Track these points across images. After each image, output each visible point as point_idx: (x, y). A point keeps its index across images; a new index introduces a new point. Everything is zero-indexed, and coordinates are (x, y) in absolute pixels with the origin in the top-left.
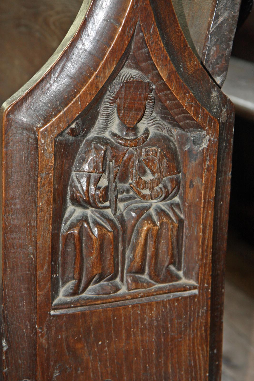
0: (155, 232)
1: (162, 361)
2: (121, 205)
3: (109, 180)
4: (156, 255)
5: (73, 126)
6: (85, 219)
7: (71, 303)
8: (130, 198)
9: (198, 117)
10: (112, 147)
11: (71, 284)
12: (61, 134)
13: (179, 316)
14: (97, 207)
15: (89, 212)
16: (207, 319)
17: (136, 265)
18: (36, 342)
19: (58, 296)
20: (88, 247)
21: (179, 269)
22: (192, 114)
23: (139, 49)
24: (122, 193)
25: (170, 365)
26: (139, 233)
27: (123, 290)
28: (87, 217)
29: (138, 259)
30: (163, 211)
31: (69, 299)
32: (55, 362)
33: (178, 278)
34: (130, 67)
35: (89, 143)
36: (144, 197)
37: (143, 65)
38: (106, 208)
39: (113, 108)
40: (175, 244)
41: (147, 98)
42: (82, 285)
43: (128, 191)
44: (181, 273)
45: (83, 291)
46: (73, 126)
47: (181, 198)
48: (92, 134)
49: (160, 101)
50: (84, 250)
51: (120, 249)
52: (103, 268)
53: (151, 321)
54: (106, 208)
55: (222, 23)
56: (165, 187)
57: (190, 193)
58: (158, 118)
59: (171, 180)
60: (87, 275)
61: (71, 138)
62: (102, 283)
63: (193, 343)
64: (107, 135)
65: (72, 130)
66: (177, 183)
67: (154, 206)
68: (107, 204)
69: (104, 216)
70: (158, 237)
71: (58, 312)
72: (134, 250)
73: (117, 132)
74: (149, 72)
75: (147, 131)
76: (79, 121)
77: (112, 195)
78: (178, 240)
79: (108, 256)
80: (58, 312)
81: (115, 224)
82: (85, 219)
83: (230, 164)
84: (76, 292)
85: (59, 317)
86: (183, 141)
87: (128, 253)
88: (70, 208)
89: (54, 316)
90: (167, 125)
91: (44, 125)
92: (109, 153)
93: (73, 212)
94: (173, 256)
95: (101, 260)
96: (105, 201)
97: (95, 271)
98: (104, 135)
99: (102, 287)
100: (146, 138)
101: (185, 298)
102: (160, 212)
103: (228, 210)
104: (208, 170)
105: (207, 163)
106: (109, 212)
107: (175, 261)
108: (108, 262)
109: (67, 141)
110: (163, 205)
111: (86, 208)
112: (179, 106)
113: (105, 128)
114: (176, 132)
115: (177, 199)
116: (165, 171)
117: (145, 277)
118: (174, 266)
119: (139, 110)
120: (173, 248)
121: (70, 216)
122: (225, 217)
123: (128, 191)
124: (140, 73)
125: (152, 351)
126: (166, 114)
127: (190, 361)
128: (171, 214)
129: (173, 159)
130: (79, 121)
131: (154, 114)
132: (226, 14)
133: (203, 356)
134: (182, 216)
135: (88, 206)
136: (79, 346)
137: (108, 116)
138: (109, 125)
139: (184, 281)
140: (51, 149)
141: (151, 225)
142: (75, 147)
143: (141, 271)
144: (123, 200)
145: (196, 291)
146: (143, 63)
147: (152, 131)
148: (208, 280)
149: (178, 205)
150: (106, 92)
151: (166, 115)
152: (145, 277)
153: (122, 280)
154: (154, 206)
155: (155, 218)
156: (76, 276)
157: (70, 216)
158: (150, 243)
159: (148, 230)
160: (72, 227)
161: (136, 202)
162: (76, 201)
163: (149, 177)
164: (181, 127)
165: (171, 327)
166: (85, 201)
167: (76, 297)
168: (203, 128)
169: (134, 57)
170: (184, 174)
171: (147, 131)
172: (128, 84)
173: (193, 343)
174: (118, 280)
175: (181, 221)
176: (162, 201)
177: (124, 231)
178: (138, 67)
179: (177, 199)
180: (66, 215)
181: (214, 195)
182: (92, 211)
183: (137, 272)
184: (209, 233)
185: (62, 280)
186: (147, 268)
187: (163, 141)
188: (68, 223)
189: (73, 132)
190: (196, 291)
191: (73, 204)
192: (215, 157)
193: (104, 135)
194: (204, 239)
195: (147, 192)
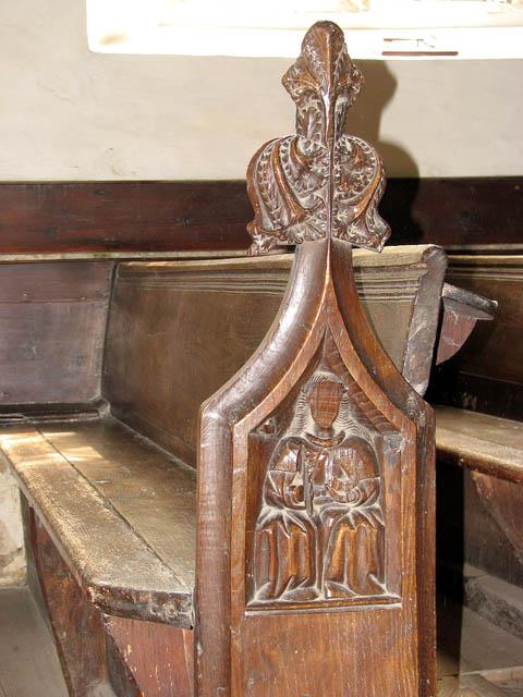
0: (352, 536)
1: (364, 679)
2: (317, 508)
3: (304, 479)
4: (355, 560)
5: (267, 423)
6: (280, 518)
7: (266, 605)
8: (326, 501)
9: (392, 418)
10: (306, 447)
11: (265, 587)
12: (254, 430)
13: (382, 632)
14: (292, 507)
15: (285, 512)
16: (413, 638)
17: (334, 570)
18: (230, 644)
19: (253, 597)
20: (282, 548)
21: (382, 581)
22: (386, 414)
23: (330, 351)
24: (318, 495)
25: (373, 687)
26: (335, 537)
27: (321, 597)
28: (282, 517)
29: (335, 564)
30: (360, 514)
31: (264, 602)
32: (250, 668)
33: (381, 591)
34: (323, 369)
35: (284, 443)
36: (341, 500)
37: (335, 367)
38: (301, 508)
39: (307, 409)
40: (375, 551)
41: (340, 399)
42: (278, 589)
43: (324, 493)
44: (384, 586)
45: (279, 595)
46: (267, 423)
47: (380, 504)
48: (288, 435)
49: (355, 403)
50: (279, 550)
51: (317, 553)
52: (298, 571)
53: (351, 633)
54: (301, 508)
55: (420, 332)
56: (363, 491)
57: (389, 498)
58: (355, 422)
59: (369, 483)
60: (282, 576)
61: (266, 436)
62: (298, 588)
63: (399, 664)
64: (302, 436)
65: (266, 427)
66: (377, 488)
67: (351, 511)
68: (302, 504)
69: (301, 518)
70: (355, 542)
71: (252, 614)
72: (331, 555)
73: (313, 433)
74: (341, 373)
75: (343, 434)
76: (273, 419)
77: (307, 494)
78: (379, 551)
79: (303, 558)
80: (252, 614)
81: (310, 525)
82: (280, 518)
83: (434, 472)
84: (271, 595)
85: (253, 618)
86: (379, 441)
87: (325, 559)
88: (265, 508)
89: (248, 617)
90: (363, 428)
91: (238, 421)
92: (303, 453)
93: (268, 511)
94: (373, 564)
95: (295, 561)
96: (301, 500)
97: (290, 573)
98: (265, 504)
99: (298, 592)
100: (341, 439)
101: (388, 611)
102: (358, 517)
103: (434, 521)
104: (406, 473)
105: (405, 467)
106: (304, 513)
107: (378, 569)
108: (304, 565)
109: (261, 439)
110: (360, 509)
111: (281, 508)
112: (373, 407)
113: (300, 429)
114: (373, 436)
115: (377, 505)
116: (362, 474)
117: (345, 585)
118: (376, 576)
119: (333, 411)
120: (372, 555)
121: (266, 515)
122: (432, 529)
123: (324, 493)
124: (333, 374)
125: (353, 668)
126: (361, 416)
127: (397, 685)
128: (370, 519)
129: (371, 459)
130: (273, 419)
131: (350, 417)
132: (424, 324)
133: (412, 682)
134: (383, 523)
135: (281, 504)
136: (274, 653)
137: (302, 416)
138: (305, 424)
139: (387, 594)
140: (245, 443)
141: (348, 529)
142: (271, 444)
143: (340, 579)
144: (318, 503)
145: (399, 605)
146: (336, 364)
147: (349, 433)
148: (413, 593)
149: (377, 510)
150: (299, 393)
151: (362, 417)
152: (345, 585)
153: (320, 587)
154: (351, 511)
155: (352, 522)
156: (271, 578)
157: (266, 515)
158: (348, 548)
159: (345, 533)
160: (266, 525)
161: (334, 505)
162: (271, 501)
163: (345, 479)
164: (377, 430)
165: (374, 643)
166: (279, 499)
167: (272, 601)
168: (398, 431)
169: (326, 359)
170: (383, 479)
171: (343, 434)
172: (321, 384)
173: (399, 664)
174: (315, 587)
175: (381, 528)
176: (361, 504)
177: (321, 534)
178: (331, 370)
179: (377, 505)
180: (261, 515)
181: (413, 501)
182: (288, 512)
183: (334, 579)
184: (411, 541)
185: (257, 581)
186: (345, 576)
187: (356, 443)
188: (263, 522)
189: (267, 430)
190: (399, 605)
191: (268, 504)
192: (413, 460)
193: (265, 504)
194: (405, 547)
195: (342, 493)
